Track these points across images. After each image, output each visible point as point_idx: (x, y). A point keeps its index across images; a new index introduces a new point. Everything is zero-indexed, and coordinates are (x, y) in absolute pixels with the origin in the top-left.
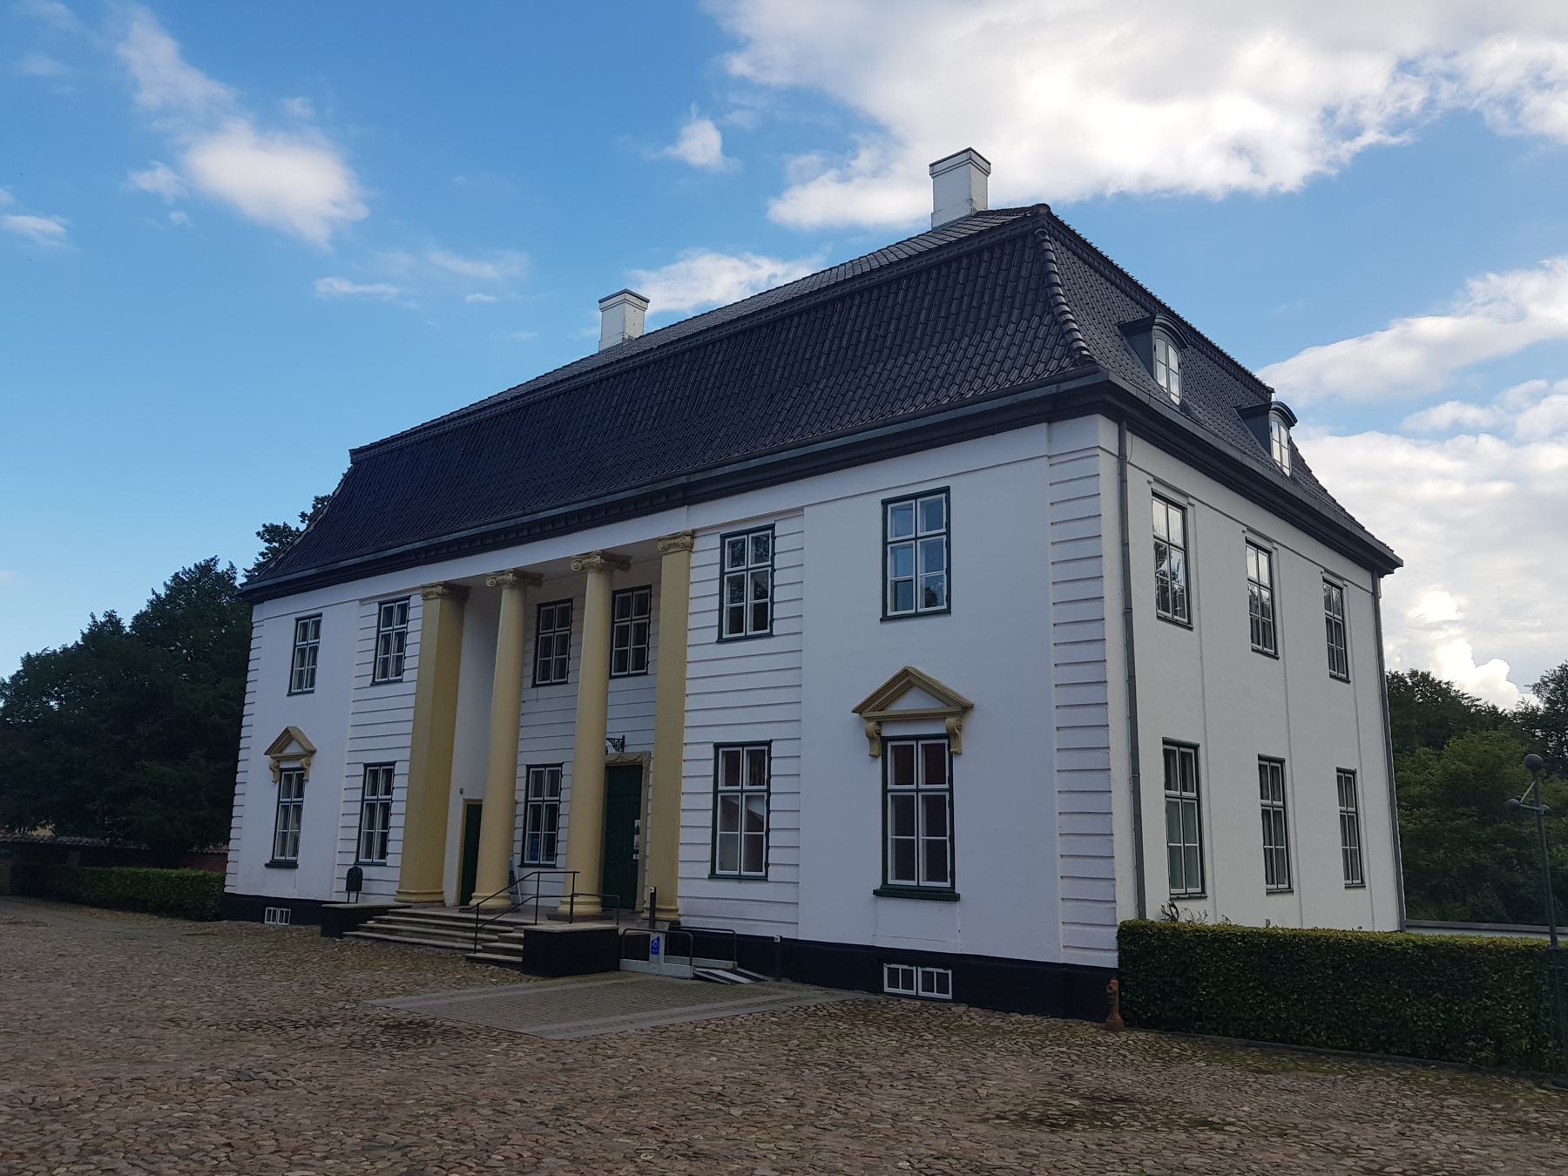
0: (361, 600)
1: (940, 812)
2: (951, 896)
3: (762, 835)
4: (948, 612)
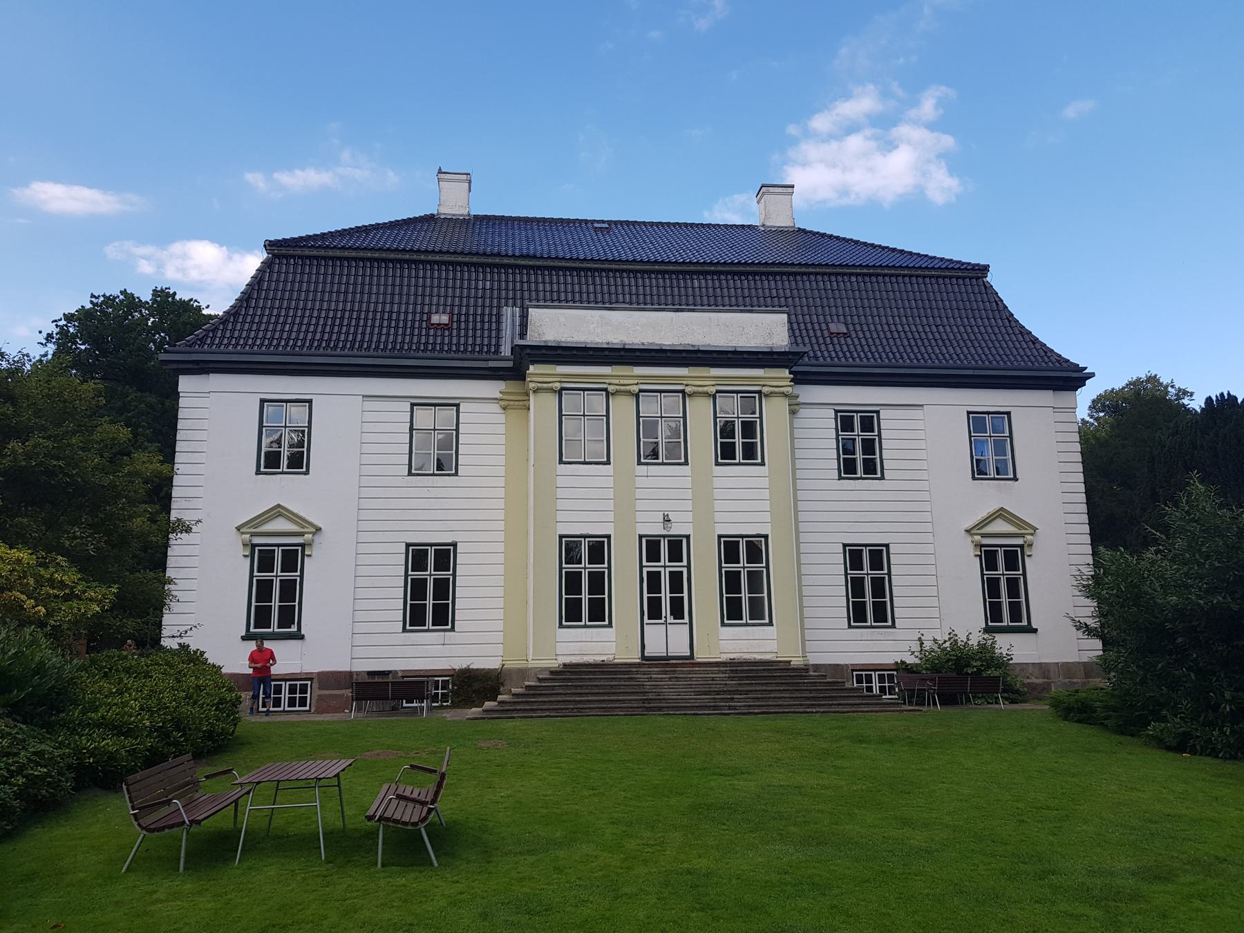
0: (364, 396)
1: (290, 590)
2: (299, 636)
3: (589, 595)
4: (307, 473)
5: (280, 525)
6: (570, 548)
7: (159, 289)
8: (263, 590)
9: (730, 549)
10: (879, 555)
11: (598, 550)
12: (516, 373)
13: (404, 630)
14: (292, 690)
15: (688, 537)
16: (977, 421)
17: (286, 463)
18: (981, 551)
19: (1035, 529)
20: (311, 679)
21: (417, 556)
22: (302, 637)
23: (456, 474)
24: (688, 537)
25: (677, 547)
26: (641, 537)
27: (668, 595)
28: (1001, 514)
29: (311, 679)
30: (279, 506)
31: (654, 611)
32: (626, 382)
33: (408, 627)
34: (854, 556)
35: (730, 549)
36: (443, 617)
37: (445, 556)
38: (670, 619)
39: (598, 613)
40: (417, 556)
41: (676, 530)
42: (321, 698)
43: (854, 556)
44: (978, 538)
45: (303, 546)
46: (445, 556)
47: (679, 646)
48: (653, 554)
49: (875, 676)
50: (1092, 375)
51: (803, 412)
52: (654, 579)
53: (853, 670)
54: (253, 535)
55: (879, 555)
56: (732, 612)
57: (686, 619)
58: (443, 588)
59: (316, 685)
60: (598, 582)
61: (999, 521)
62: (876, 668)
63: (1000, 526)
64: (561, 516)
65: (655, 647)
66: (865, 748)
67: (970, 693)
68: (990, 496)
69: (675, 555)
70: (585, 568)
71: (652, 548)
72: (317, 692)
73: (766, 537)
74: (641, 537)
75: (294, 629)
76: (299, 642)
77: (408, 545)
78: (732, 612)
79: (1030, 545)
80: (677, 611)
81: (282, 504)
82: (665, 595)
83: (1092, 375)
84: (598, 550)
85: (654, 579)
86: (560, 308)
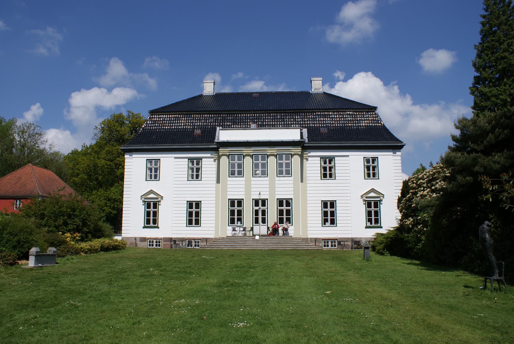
2: (158, 227)
4: (159, 180)
5: (152, 196)
6: (232, 202)
8: (148, 214)
9: (281, 202)
10: (333, 204)
11: (240, 203)
12: (216, 150)
13: (187, 226)
14: (156, 242)
15: (267, 199)
17: (288, 161)
18: (366, 202)
19: (383, 195)
20: (161, 239)
21: (190, 204)
22: (382, 227)
23: (201, 180)
24: (267, 199)
25: (264, 202)
26: (253, 199)
27: (259, 217)
28: (373, 190)
29: (161, 239)
30: (151, 190)
31: (257, 221)
32: (249, 152)
33: (188, 225)
35: (281, 202)
36: (197, 222)
37: (198, 204)
38: (261, 224)
40: (190, 204)
41: (262, 197)
42: (164, 245)
44: (364, 198)
45: (158, 201)
46: (198, 204)
48: (257, 204)
49: (155, 241)
53: (148, 239)
54: (145, 198)
55: (333, 204)
57: (266, 224)
58: (198, 214)
59: (163, 241)
60: (240, 213)
62: (194, 239)
63: (372, 194)
64: (228, 193)
66: (444, 275)
67: (343, 249)
68: (372, 184)
69: (264, 204)
70: (194, 210)
71: (256, 202)
72: (163, 243)
73: (292, 199)
74: (253, 199)
76: (381, 229)
77: (187, 201)
79: (382, 201)
82: (260, 216)
84: (240, 203)
85: (257, 212)
86: (229, 130)
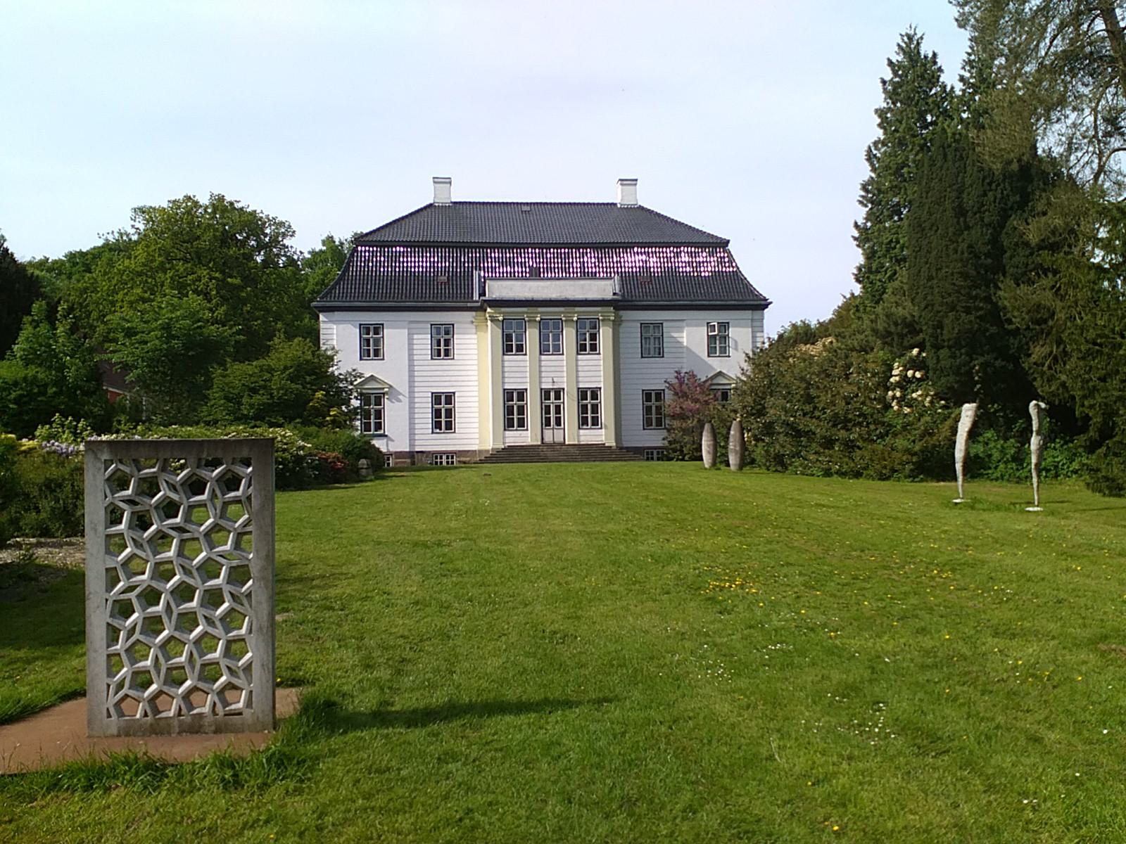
7: (856, 272)
11: (521, 394)
16: (365, 329)
31: (548, 423)
34: (437, 398)
35: (583, 394)
39: (522, 423)
43: (437, 398)
47: (559, 439)
50: (771, 303)
51: (624, 325)
52: (548, 408)
56: (583, 422)
61: (720, 378)
62: (444, 452)
65: (548, 438)
69: (558, 397)
75: (382, 432)
78: (583, 422)
80: (558, 422)
81: (724, 371)
83: (771, 303)
84: (521, 394)
